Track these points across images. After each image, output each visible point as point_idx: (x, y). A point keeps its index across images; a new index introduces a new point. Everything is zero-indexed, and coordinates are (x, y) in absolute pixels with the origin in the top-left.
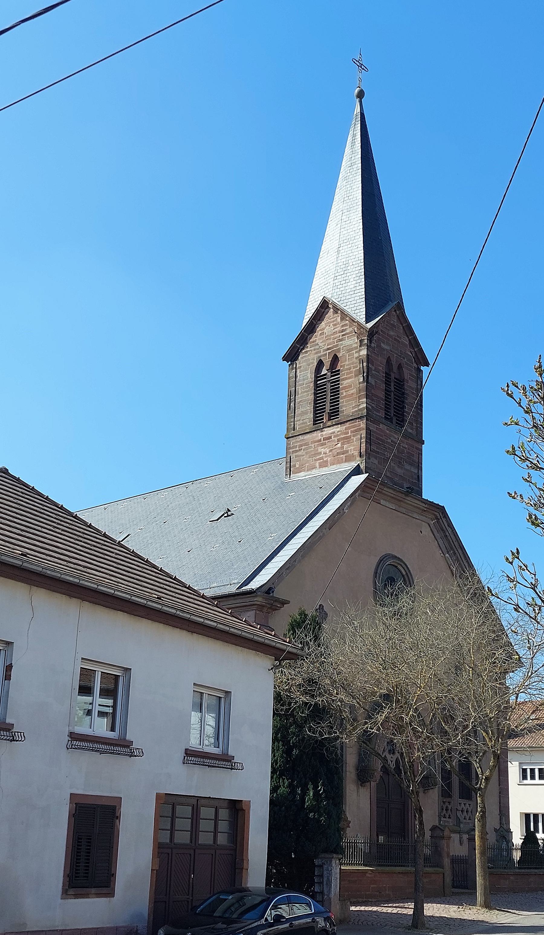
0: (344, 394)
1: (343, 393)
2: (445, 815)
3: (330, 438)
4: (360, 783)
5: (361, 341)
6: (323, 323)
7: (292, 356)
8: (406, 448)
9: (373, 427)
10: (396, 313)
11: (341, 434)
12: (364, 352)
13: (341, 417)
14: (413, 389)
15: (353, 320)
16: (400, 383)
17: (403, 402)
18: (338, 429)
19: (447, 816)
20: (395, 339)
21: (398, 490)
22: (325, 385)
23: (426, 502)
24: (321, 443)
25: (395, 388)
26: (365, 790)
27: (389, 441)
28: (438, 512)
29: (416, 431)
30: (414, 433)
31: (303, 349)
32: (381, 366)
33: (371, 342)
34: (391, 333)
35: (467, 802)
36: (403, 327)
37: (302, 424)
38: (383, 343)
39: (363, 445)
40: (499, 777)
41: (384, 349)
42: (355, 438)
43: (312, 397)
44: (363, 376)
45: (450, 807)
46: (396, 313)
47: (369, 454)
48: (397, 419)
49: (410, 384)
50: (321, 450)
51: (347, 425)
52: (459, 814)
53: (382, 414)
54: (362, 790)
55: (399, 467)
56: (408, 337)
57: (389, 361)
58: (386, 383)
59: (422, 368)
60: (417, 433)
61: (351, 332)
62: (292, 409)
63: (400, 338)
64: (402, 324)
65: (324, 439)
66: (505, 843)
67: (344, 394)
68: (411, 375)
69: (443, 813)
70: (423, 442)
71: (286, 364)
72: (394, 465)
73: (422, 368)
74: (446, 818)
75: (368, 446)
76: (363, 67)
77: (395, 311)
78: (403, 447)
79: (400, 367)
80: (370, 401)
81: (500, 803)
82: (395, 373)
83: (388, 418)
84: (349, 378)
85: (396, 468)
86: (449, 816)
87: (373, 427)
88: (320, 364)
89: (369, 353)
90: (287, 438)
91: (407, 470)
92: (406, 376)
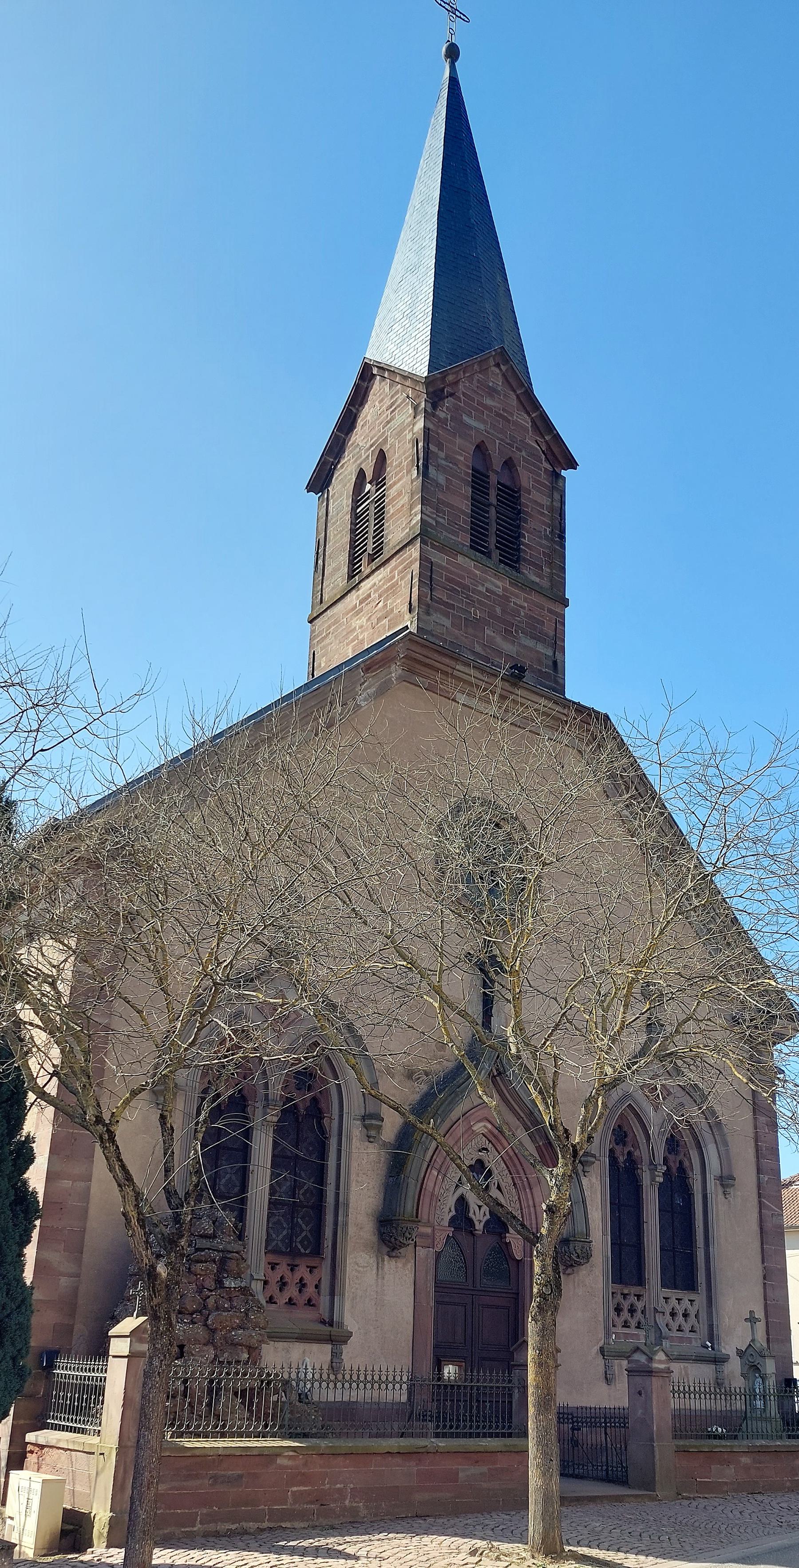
0: (391, 512)
1: (390, 510)
2: (626, 1322)
3: (369, 595)
4: (385, 1249)
5: (415, 408)
6: (366, 406)
7: (320, 482)
8: (524, 608)
9: (439, 558)
10: (501, 370)
11: (383, 584)
12: (420, 424)
13: (387, 553)
14: (542, 506)
15: (406, 376)
16: (511, 496)
17: (519, 527)
18: (380, 577)
19: (633, 1323)
20: (498, 415)
21: (488, 670)
22: (368, 509)
23: (568, 704)
24: (356, 612)
25: (498, 500)
26: (400, 1265)
27: (480, 588)
28: (593, 723)
29: (551, 581)
30: (545, 583)
31: (339, 462)
32: (461, 455)
33: (435, 406)
34: (489, 402)
35: (686, 1296)
36: (518, 396)
37: (333, 588)
38: (469, 415)
39: (415, 590)
40: (762, 1244)
41: (470, 427)
42: (403, 582)
43: (347, 539)
44: (418, 466)
45: (639, 1305)
46: (501, 370)
47: (428, 606)
48: (501, 555)
49: (534, 497)
50: (356, 623)
51: (393, 563)
52: (661, 1321)
53: (464, 539)
54: (390, 1265)
55: (505, 639)
56: (529, 415)
57: (481, 449)
58: (473, 487)
59: (563, 473)
60: (552, 585)
61: (404, 400)
62: (320, 569)
63: (512, 415)
64: (514, 391)
65: (361, 603)
66: (760, 1380)
67: (391, 512)
68: (538, 482)
69: (623, 1319)
70: (565, 603)
71: (314, 497)
72: (492, 634)
73: (563, 473)
74: (629, 1327)
75: (427, 590)
76: (457, 13)
77: (498, 365)
78: (515, 603)
79: (509, 464)
80: (430, 509)
81: (765, 1299)
82: (497, 473)
83: (478, 544)
84: (399, 480)
85: (499, 640)
86: (639, 1323)
87: (439, 558)
88: (361, 474)
89: (431, 426)
90: (311, 622)
91: (525, 647)
92: (525, 478)
